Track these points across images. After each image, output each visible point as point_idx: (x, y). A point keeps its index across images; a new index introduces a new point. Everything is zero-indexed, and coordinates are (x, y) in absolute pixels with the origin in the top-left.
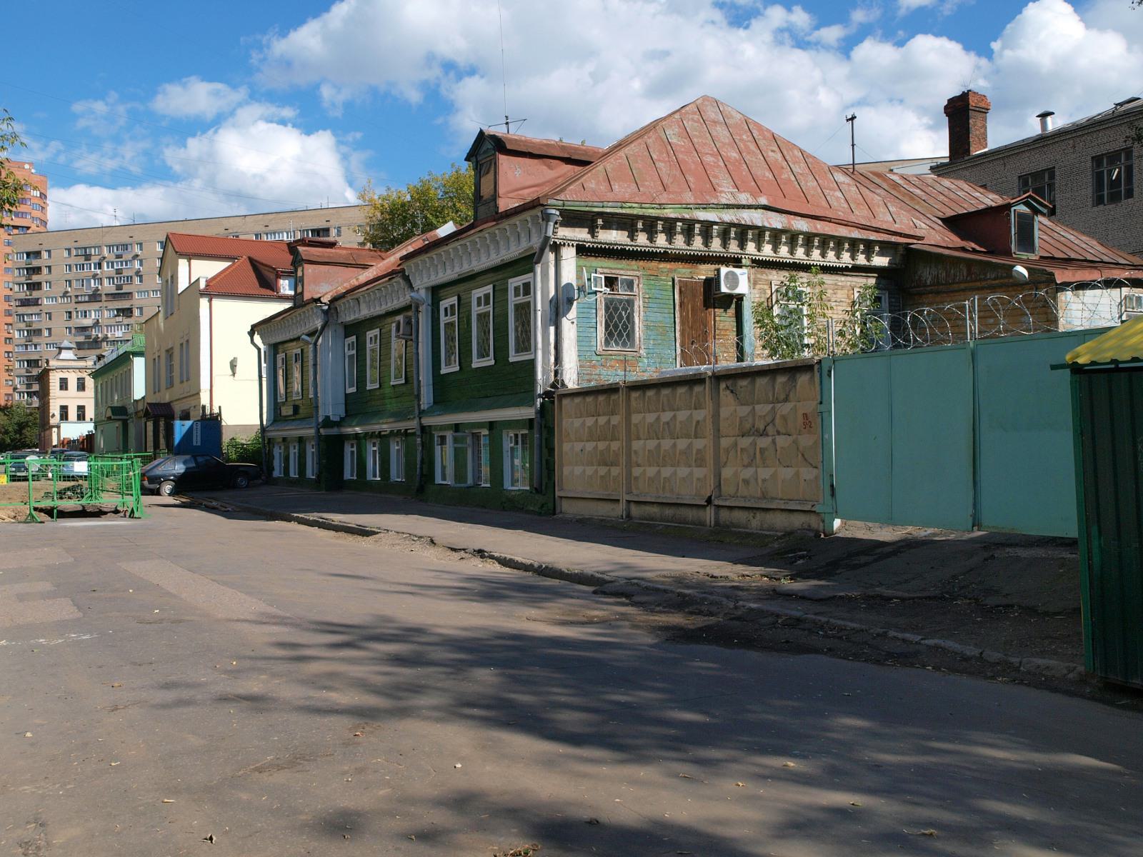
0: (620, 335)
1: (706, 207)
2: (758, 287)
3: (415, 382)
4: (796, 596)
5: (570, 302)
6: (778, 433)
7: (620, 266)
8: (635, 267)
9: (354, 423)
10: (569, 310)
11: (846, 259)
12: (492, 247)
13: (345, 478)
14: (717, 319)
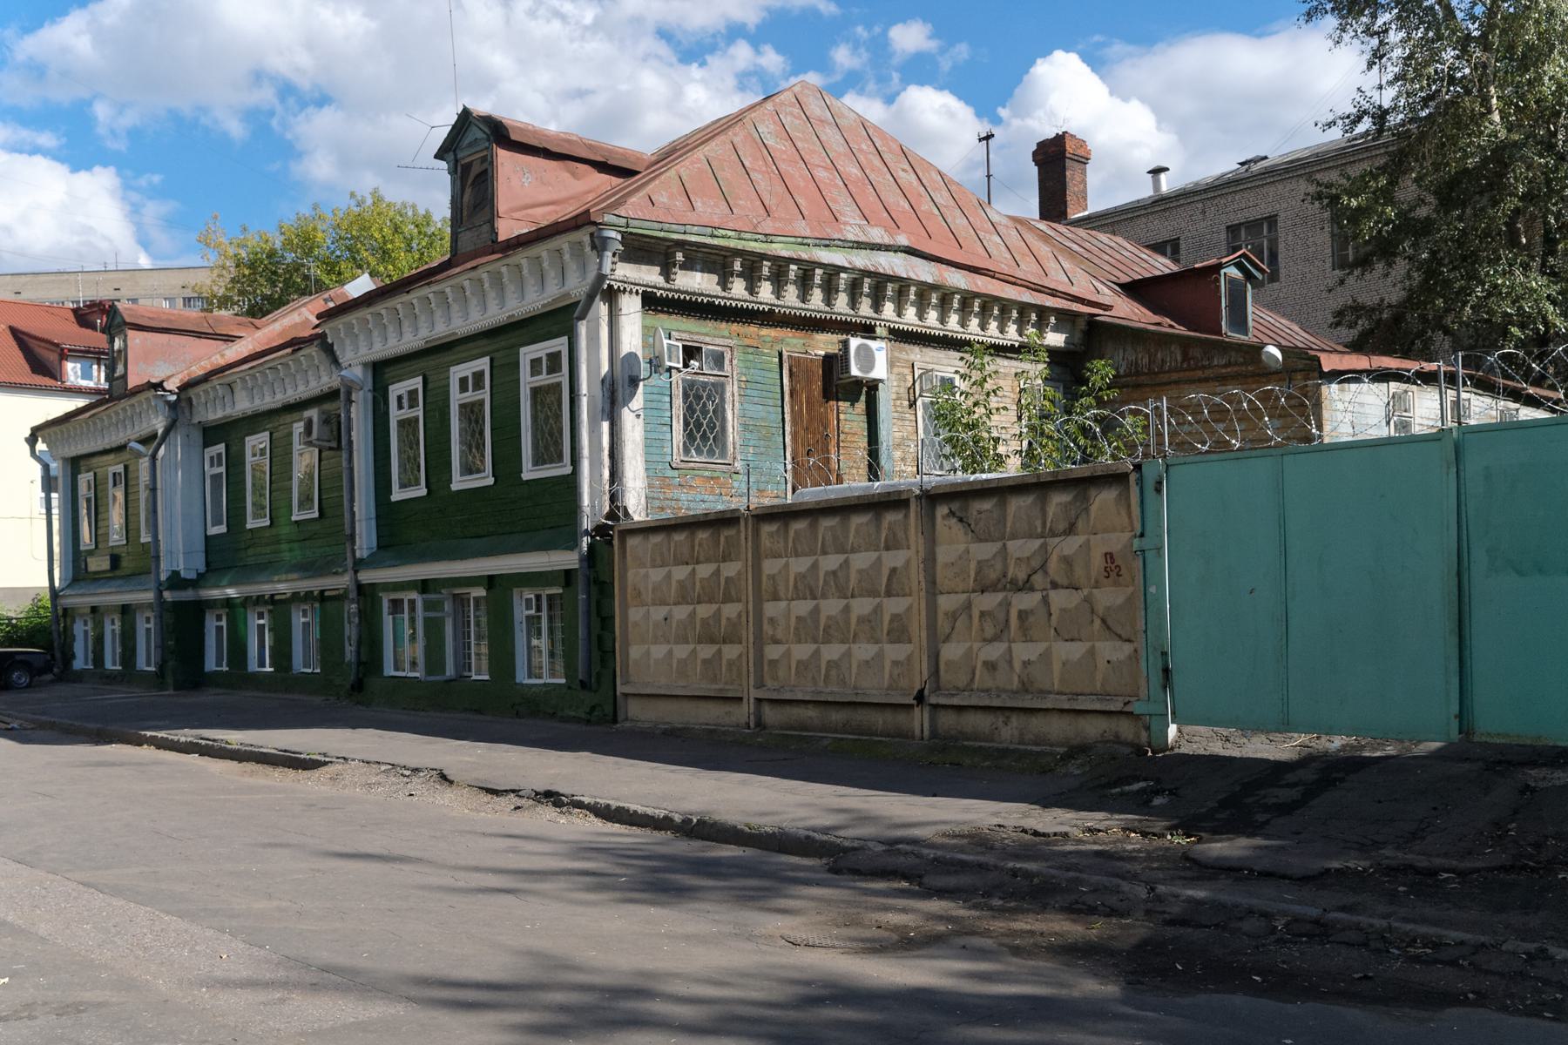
0: (704, 438)
1: (828, 243)
2: (896, 370)
3: (347, 516)
4: (1251, 871)
5: (634, 382)
6: (1055, 585)
7: (704, 330)
8: (726, 333)
9: (225, 582)
10: (633, 395)
11: (1012, 335)
12: (348, 342)
13: (207, 669)
14: (842, 416)
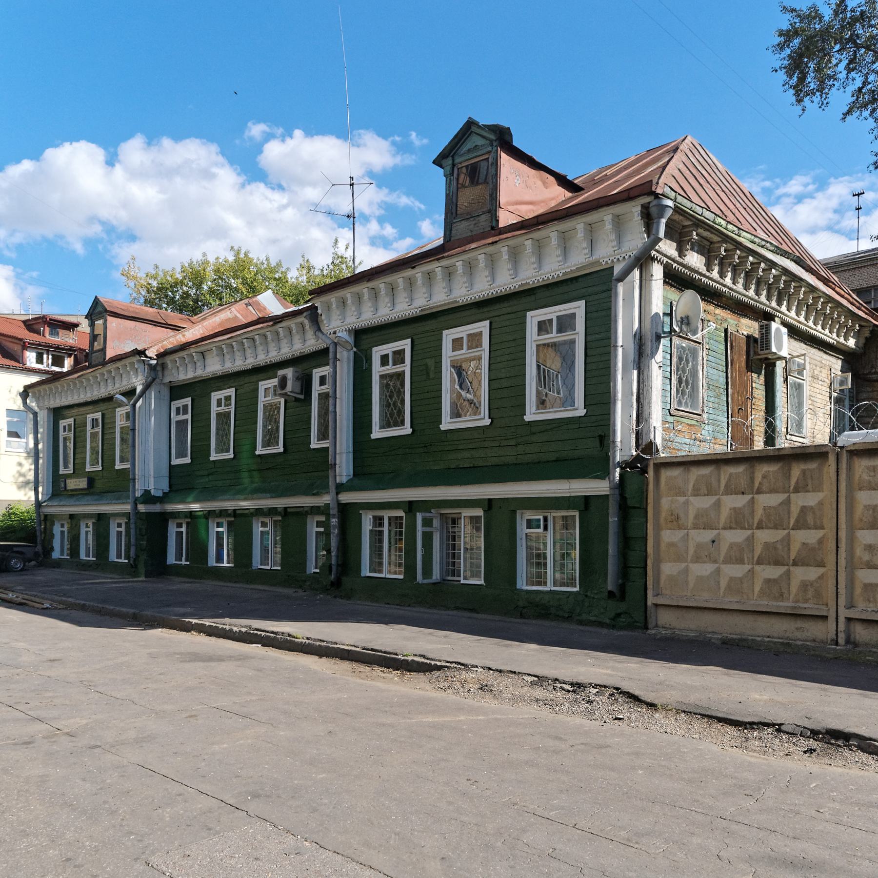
9: (189, 500)
14: (754, 385)
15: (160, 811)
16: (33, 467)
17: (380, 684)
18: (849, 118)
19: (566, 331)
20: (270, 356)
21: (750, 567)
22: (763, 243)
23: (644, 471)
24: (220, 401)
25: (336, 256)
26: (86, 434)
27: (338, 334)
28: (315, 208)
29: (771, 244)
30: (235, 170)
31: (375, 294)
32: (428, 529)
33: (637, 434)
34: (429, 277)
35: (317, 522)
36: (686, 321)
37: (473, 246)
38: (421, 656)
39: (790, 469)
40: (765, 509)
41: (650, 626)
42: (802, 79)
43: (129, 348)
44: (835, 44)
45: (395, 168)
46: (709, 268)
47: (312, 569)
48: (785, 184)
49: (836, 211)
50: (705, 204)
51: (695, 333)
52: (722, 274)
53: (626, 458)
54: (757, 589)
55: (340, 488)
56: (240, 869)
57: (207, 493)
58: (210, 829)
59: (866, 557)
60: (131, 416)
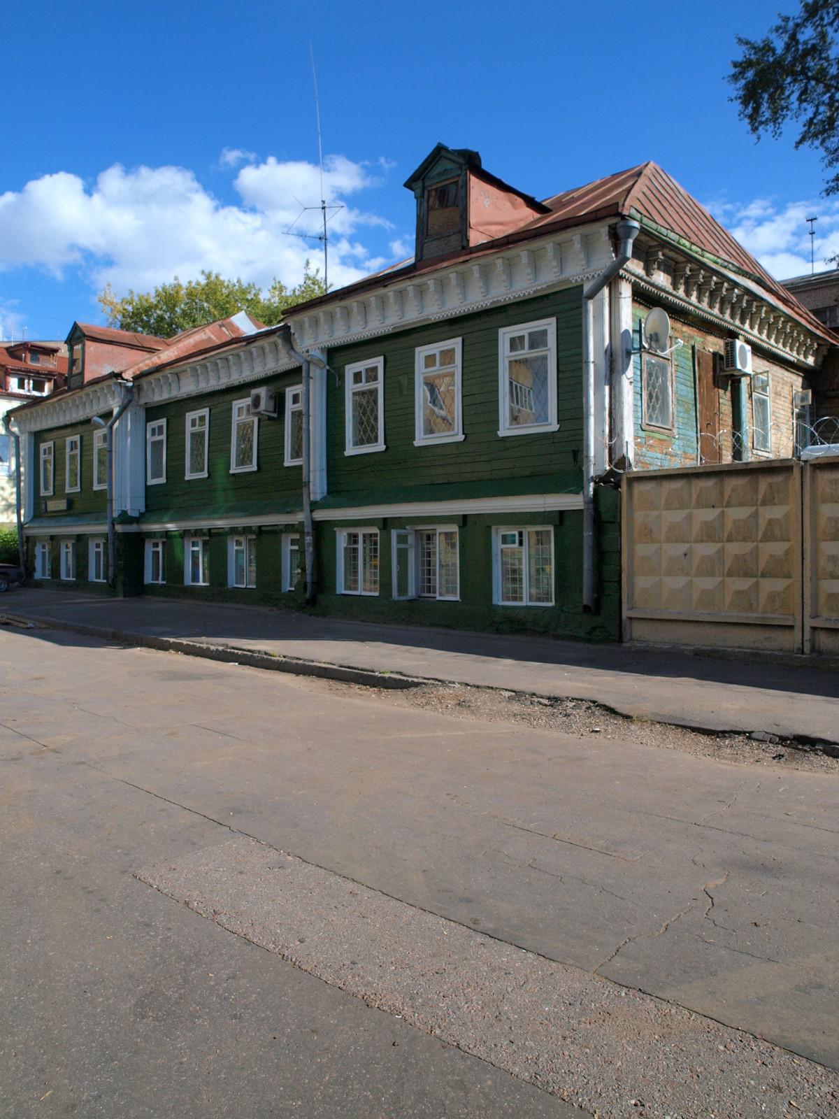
9: (166, 519)
13: (145, 582)
14: (721, 401)
15: (145, 826)
16: (15, 490)
17: (357, 701)
18: (801, 146)
19: (537, 347)
20: (243, 375)
21: (721, 579)
22: (726, 264)
23: (617, 485)
24: (195, 421)
25: (308, 277)
26: (65, 457)
27: (311, 353)
28: (287, 230)
29: (733, 265)
30: (209, 195)
31: (347, 313)
32: (403, 546)
33: (610, 449)
34: (401, 294)
35: (292, 540)
36: (654, 337)
37: (444, 264)
38: (397, 673)
39: (757, 483)
40: (734, 522)
41: (624, 640)
42: (756, 110)
43: (106, 371)
44: (787, 77)
45: (365, 189)
46: (675, 287)
47: (287, 587)
48: (746, 207)
49: (793, 234)
50: (670, 227)
51: (663, 350)
52: (688, 293)
53: (599, 473)
54: (728, 600)
55: (314, 506)
56: (225, 883)
57: (183, 512)
58: (194, 844)
59: (830, 568)
60: (108, 438)
